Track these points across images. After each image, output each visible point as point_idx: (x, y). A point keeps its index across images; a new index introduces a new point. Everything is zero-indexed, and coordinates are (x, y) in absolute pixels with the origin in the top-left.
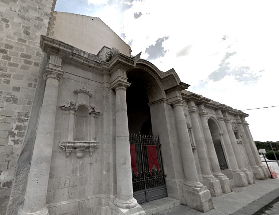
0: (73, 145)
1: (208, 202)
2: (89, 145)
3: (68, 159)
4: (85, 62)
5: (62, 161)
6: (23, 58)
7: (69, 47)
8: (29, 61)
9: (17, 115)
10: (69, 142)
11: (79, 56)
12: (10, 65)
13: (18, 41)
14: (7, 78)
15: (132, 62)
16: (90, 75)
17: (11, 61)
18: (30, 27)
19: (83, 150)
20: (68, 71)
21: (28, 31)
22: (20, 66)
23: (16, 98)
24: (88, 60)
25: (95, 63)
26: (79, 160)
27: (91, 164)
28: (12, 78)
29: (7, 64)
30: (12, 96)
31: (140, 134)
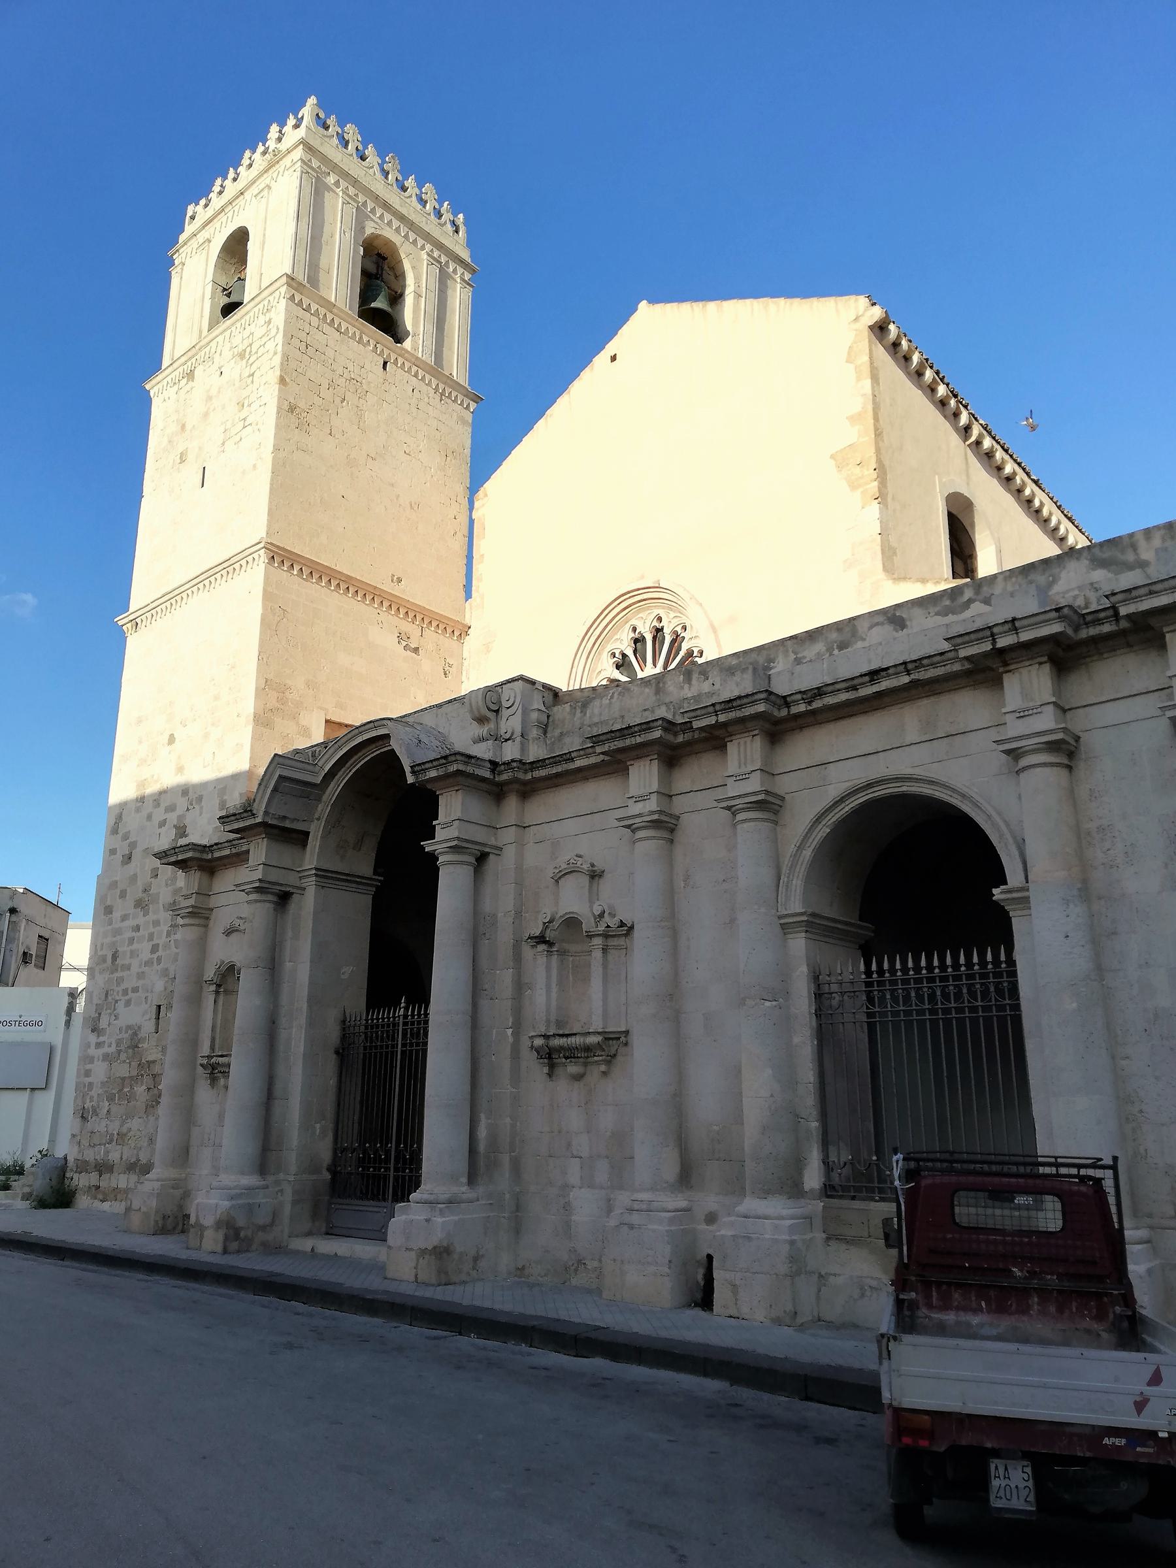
1: (413, 1255)
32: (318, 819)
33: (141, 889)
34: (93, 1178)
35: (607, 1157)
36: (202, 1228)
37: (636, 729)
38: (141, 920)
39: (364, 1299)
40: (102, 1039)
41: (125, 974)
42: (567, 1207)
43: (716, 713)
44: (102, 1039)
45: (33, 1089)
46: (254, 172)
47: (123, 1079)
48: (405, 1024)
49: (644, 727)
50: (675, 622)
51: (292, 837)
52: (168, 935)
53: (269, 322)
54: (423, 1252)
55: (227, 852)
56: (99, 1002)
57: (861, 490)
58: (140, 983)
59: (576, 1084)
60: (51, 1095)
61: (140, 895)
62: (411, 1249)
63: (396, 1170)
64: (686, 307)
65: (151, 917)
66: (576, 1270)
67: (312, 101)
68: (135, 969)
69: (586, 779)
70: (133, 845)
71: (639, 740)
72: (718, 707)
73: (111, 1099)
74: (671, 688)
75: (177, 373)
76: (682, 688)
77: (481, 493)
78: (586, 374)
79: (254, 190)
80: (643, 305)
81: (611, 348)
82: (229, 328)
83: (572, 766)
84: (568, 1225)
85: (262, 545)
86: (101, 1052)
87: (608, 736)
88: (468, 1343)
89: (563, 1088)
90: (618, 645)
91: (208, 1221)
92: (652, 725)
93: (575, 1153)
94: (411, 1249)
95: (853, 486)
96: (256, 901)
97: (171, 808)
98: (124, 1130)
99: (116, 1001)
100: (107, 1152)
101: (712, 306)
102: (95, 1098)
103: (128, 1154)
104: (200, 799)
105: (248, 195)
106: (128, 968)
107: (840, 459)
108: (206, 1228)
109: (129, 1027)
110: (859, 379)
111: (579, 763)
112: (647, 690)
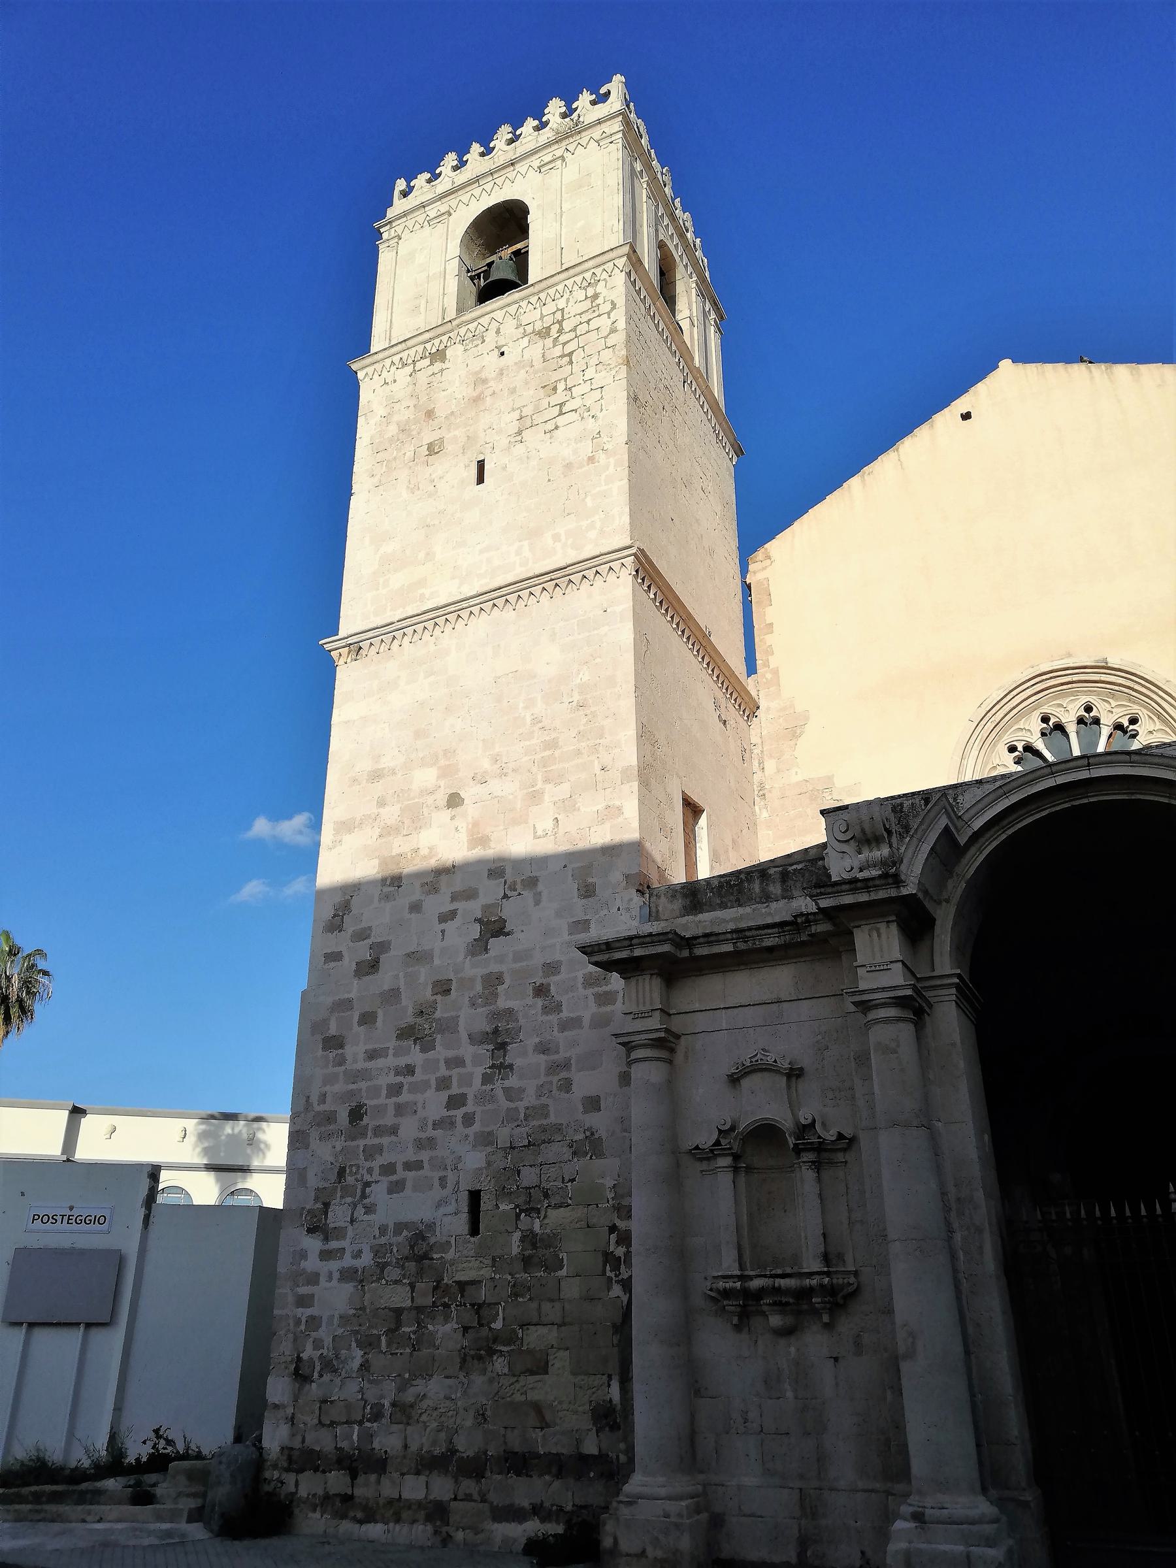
0: (738, 1284)
2: (746, 1285)
4: (742, 946)
5: (718, 1343)
6: (590, 991)
7: (655, 939)
9: (610, 1195)
10: (724, 1277)
11: (712, 938)
12: (564, 1026)
14: (564, 1074)
17: (565, 1014)
18: (590, 866)
20: (697, 1006)
21: (590, 880)
22: (586, 1022)
24: (748, 934)
26: (782, 1342)
27: (836, 1359)
28: (573, 1068)
29: (556, 1029)
30: (588, 1134)
32: (947, 901)
33: (410, 1010)
34: (336, 1481)
38: (416, 1056)
40: (334, 1244)
41: (385, 1140)
44: (334, 1244)
45: (88, 1325)
46: (546, 134)
47: (398, 1312)
50: (1119, 712)
51: (915, 922)
52: (487, 1079)
53: (596, 296)
55: (729, 948)
56: (322, 1184)
58: (425, 1156)
60: (117, 1336)
61: (410, 1019)
65: (441, 1052)
67: (618, 79)
68: (409, 1128)
70: (381, 947)
73: (368, 1343)
75: (412, 352)
77: (760, 554)
79: (535, 161)
82: (516, 302)
86: (334, 1265)
90: (1021, 735)
96: (899, 1019)
97: (470, 894)
98: (409, 1396)
99: (367, 1184)
100: (369, 1436)
102: (328, 1341)
103: (421, 1439)
104: (532, 882)
105: (522, 167)
106: (394, 1131)
109: (399, 1227)
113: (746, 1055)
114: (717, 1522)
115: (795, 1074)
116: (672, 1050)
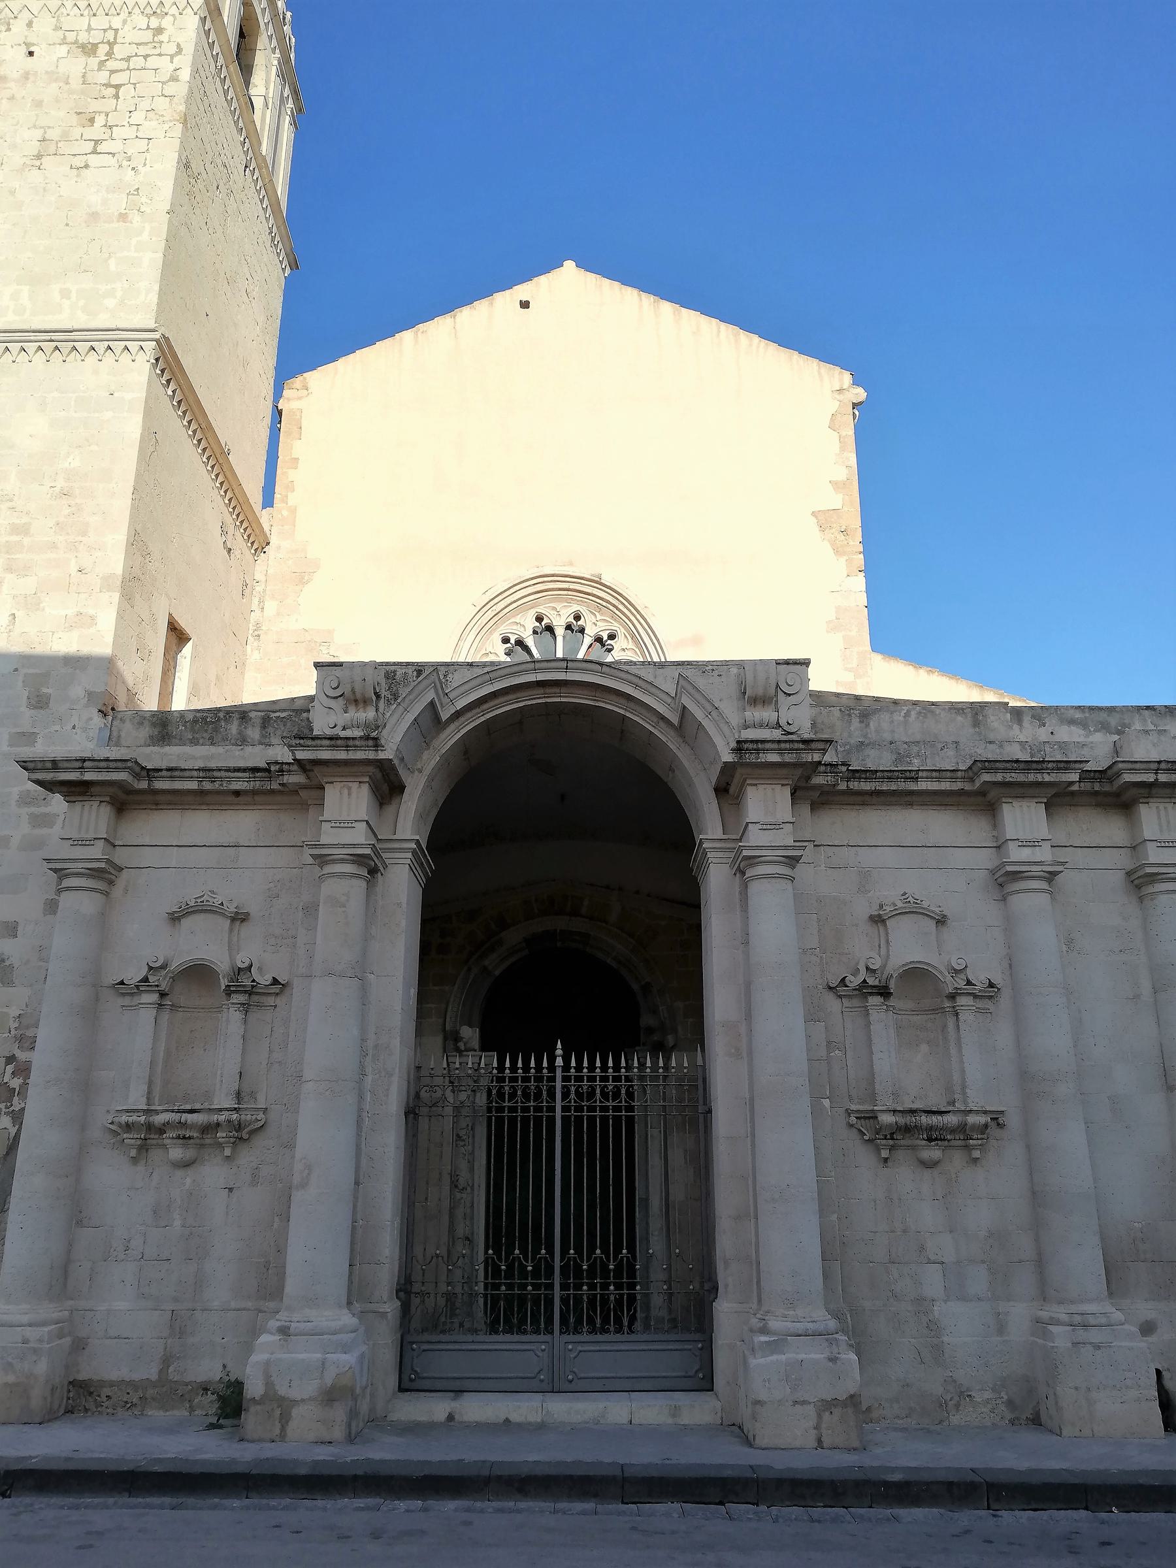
0: (235, 1116)
1: (810, 1410)
3: (140, 1168)
8: (46, 815)
13: (10, 745)
15: (371, 743)
16: (242, 823)
19: (190, 1138)
21: (45, 690)
23: (7, 963)
24: (216, 774)
25: (247, 775)
26: (179, 1173)
27: (231, 1190)
31: (559, 1052)
32: (420, 771)
35: (983, 1262)
36: (283, 1407)
37: (1050, 765)
39: (886, 1484)
42: (933, 1327)
43: (1156, 772)
48: (566, 1079)
49: (1062, 765)
51: (387, 785)
54: (828, 1405)
57: (846, 558)
59: (927, 1174)
62: (804, 1403)
63: (564, 1287)
64: (631, 294)
66: (957, 1406)
69: (911, 804)
71: (1047, 778)
72: (1163, 766)
74: (996, 724)
76: (1011, 727)
77: (297, 382)
78: (481, 306)
80: (569, 265)
81: (522, 291)
83: (912, 786)
84: (938, 1350)
85: (157, 336)
87: (1008, 765)
88: (1016, 1519)
89: (905, 1176)
91: (303, 1389)
92: (1073, 765)
93: (933, 1258)
94: (804, 1403)
95: (838, 552)
101: (667, 307)
107: (824, 520)
108: (295, 1403)
110: (843, 449)
111: (923, 785)
112: (959, 718)
113: (190, 896)
114: (80, 1345)
115: (240, 918)
116: (111, 883)
